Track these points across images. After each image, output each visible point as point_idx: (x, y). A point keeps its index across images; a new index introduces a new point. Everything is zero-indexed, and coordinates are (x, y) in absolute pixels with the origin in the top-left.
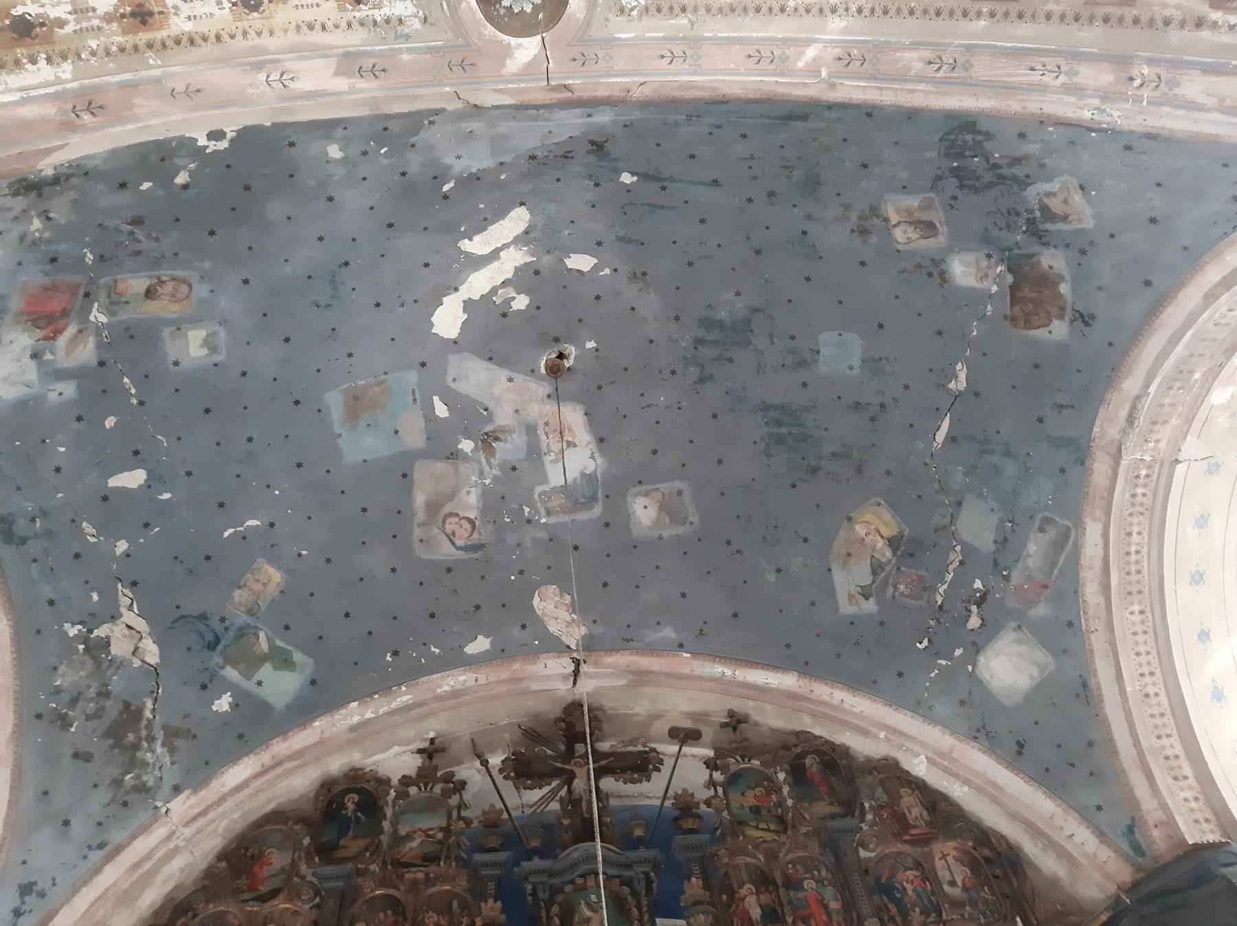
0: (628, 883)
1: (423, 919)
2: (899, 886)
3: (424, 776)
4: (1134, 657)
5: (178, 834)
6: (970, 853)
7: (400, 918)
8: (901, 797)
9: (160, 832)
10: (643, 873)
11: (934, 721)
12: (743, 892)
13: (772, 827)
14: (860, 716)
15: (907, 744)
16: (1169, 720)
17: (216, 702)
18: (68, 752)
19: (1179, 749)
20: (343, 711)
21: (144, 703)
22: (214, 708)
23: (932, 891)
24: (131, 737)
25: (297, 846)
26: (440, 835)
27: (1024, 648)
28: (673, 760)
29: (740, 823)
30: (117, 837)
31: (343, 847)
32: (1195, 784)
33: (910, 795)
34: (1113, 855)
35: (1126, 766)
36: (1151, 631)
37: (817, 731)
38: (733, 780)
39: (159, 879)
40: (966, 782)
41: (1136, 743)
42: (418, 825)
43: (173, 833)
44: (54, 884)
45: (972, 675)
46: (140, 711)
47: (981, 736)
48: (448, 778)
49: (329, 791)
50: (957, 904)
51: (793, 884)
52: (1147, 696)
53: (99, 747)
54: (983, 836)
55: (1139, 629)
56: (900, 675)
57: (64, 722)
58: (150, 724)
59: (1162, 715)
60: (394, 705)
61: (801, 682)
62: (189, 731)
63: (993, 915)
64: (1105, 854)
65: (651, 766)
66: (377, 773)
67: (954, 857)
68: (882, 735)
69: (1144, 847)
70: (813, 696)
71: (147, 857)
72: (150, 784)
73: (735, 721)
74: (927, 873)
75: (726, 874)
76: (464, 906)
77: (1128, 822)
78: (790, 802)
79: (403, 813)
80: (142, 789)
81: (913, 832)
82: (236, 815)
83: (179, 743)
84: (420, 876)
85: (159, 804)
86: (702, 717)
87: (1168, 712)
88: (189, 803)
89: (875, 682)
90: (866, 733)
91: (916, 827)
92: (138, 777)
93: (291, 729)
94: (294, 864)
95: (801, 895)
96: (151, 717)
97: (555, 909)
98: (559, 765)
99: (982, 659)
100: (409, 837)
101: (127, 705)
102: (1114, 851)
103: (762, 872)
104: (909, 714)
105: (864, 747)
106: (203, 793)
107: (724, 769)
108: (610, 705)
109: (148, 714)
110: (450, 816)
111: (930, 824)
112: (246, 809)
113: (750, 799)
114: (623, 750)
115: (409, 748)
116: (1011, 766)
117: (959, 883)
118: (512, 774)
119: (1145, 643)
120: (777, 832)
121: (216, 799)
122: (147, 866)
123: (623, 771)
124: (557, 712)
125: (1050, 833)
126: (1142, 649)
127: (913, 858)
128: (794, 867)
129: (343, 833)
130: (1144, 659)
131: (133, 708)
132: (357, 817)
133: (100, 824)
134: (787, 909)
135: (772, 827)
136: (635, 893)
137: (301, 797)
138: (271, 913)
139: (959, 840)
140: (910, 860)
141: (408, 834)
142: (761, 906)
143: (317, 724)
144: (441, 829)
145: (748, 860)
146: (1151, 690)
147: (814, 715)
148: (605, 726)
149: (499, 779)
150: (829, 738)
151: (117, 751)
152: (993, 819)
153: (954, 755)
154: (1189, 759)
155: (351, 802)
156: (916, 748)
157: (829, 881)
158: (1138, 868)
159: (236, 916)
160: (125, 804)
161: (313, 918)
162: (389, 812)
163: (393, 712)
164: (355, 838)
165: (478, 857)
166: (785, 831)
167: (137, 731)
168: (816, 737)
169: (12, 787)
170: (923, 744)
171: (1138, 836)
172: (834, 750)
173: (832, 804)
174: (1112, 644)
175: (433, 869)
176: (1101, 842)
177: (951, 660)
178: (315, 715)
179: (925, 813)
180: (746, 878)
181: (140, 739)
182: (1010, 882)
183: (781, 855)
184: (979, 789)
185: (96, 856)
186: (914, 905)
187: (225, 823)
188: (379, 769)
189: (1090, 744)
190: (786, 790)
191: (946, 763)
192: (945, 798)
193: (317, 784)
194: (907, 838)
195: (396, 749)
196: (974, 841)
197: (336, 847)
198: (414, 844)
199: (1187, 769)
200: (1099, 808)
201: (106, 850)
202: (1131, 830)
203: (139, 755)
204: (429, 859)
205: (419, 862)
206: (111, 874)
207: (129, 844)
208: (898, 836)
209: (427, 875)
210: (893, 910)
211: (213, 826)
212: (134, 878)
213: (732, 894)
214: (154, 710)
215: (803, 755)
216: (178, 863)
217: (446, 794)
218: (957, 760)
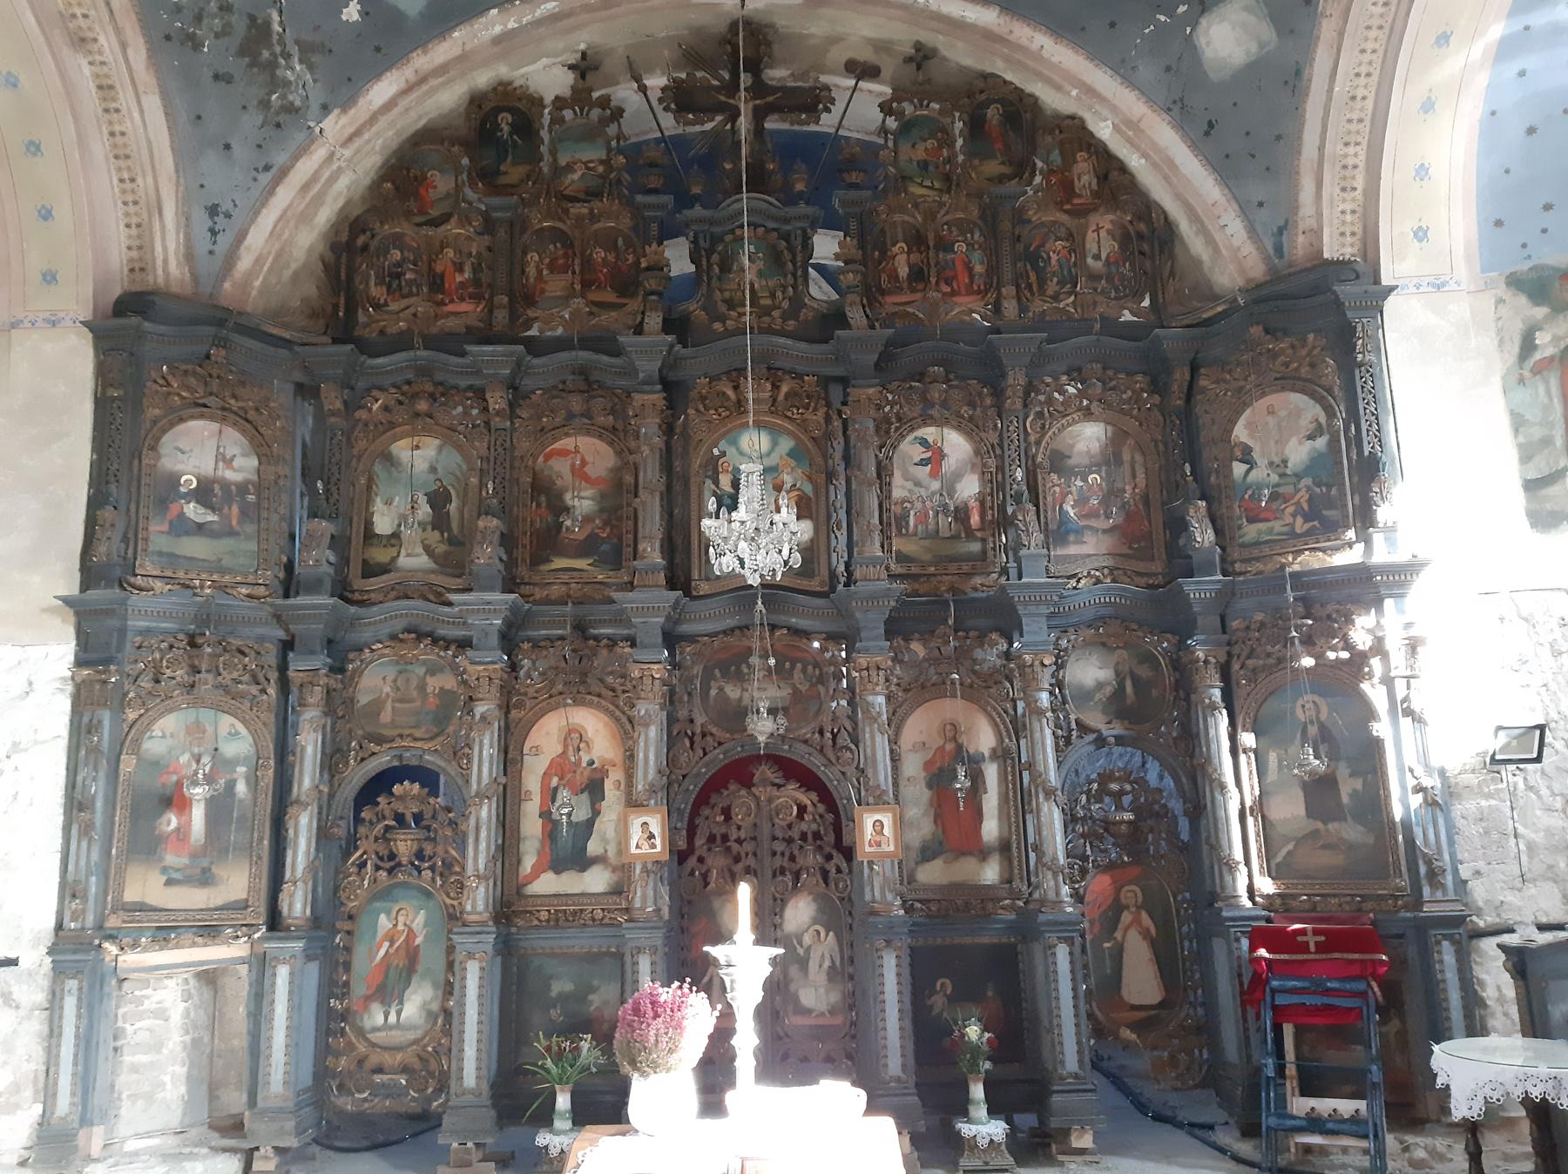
0: (786, 237)
1: (591, 254)
2: (1045, 256)
3: (579, 97)
4: (1356, 52)
5: (338, 155)
6: (1124, 227)
7: (570, 252)
8: (1075, 161)
9: (319, 154)
10: (801, 228)
11: (1130, 81)
12: (895, 249)
13: (937, 185)
14: (1055, 67)
15: (1097, 107)
16: (1366, 128)
17: (345, 10)
18: (207, 74)
19: (1361, 160)
20: (483, 20)
21: (270, 15)
22: (344, 18)
23: (1075, 263)
24: (266, 54)
25: (458, 171)
26: (601, 169)
27: (1252, 19)
28: (849, 93)
29: (904, 178)
30: (280, 159)
31: (505, 173)
32: (1360, 197)
33: (1085, 160)
34: (1254, 252)
35: (1302, 170)
36: (1387, 27)
37: (1008, 77)
38: (907, 127)
39: (329, 199)
40: (1145, 155)
41: (1321, 148)
42: (578, 156)
43: (331, 156)
44: (235, 206)
45: (1189, 39)
46: (268, 24)
47: (1176, 109)
48: (605, 102)
49: (480, 107)
50: (1094, 277)
51: (945, 245)
52: (1353, 98)
53: (236, 65)
54: (1146, 209)
55: (1375, 22)
56: (1112, 25)
57: (196, 44)
58: (281, 41)
59: (1360, 121)
60: (538, 13)
61: (1001, 21)
62: (323, 44)
63: (1125, 289)
64: (1248, 249)
65: (821, 106)
66: (528, 88)
67: (1108, 232)
68: (1074, 93)
69: (1285, 250)
70: (1012, 38)
71: (314, 178)
72: (298, 103)
73: (922, 56)
74: (1075, 241)
75: (883, 231)
76: (629, 244)
77: (1282, 223)
78: (961, 158)
79: (561, 140)
80: (290, 109)
81: (1076, 201)
82: (390, 133)
83: (316, 58)
84: (585, 211)
85: (312, 124)
86: (881, 46)
87: (1367, 122)
88: (341, 123)
89: (1083, 29)
90: (1058, 88)
91: (1080, 196)
92: (284, 96)
93: (429, 41)
94: (458, 188)
95: (950, 256)
96: (281, 30)
97: (715, 258)
98: (723, 98)
99: (1204, 22)
100: (569, 168)
101: (252, 18)
102: (1258, 249)
103: (918, 231)
104: (1110, 72)
105: (1054, 101)
106: (352, 112)
107: (899, 115)
108: (783, 23)
109: (277, 28)
110: (609, 150)
111: (1096, 194)
112: (398, 126)
113: (920, 154)
114: (793, 84)
115: (559, 59)
116: (1194, 147)
117: (1104, 256)
118: (673, 106)
119: (1376, 39)
120: (940, 190)
121: (367, 117)
122: (317, 187)
123: (792, 109)
124: (722, 27)
125: (1204, 219)
126: (1369, 46)
127: (1068, 229)
128: (949, 229)
129: (502, 159)
130: (1367, 57)
131: (259, 21)
132: (514, 142)
133: (259, 146)
134: (933, 272)
135: (937, 185)
136: (791, 249)
137: (451, 111)
138: (446, 237)
139: (1118, 213)
140: (1063, 229)
141: (568, 165)
142: (909, 267)
143: (456, 34)
144: (601, 162)
145: (906, 218)
146: (1360, 93)
147: (1008, 60)
148: (775, 47)
149: (658, 109)
150: (1018, 85)
151: (255, 70)
152: (1160, 194)
153: (1142, 125)
154: (1367, 170)
155: (504, 120)
156: (1105, 112)
157: (980, 247)
158: (1271, 269)
159: (413, 239)
160: (278, 125)
161: (487, 244)
162: (544, 134)
163: (538, 23)
164: (515, 164)
165: (639, 198)
166: (948, 192)
167: (270, 46)
168: (1005, 82)
169: (166, 114)
170: (1114, 109)
171: (1285, 238)
172: (1021, 100)
173: (1003, 163)
174: (1341, 34)
175: (597, 205)
176: (1249, 238)
177: (1170, 17)
178: (452, 24)
179: (1095, 181)
180: (900, 236)
181: (274, 55)
182: (1154, 262)
183: (939, 216)
184: (1155, 165)
185: (265, 178)
186: (1054, 274)
187: (380, 142)
188: (529, 83)
189: (1279, 138)
190: (960, 142)
191: (1131, 133)
192: (1123, 168)
193: (466, 99)
194: (1067, 207)
195: (545, 61)
196: (1133, 214)
197: (498, 173)
198: (576, 176)
199: (1360, 183)
200: (1261, 204)
201: (274, 170)
202: (1281, 231)
203: (278, 72)
204: (592, 194)
205: (582, 196)
206: (284, 195)
207: (293, 166)
208: (1059, 205)
209: (591, 211)
210: (1033, 277)
211: (368, 147)
212: (308, 199)
213: (884, 251)
214: (281, 23)
215: (985, 105)
216: (343, 182)
217: (604, 122)
218: (1142, 131)
